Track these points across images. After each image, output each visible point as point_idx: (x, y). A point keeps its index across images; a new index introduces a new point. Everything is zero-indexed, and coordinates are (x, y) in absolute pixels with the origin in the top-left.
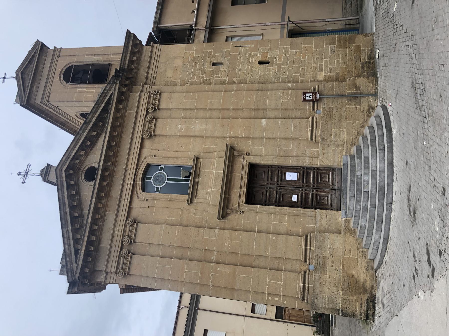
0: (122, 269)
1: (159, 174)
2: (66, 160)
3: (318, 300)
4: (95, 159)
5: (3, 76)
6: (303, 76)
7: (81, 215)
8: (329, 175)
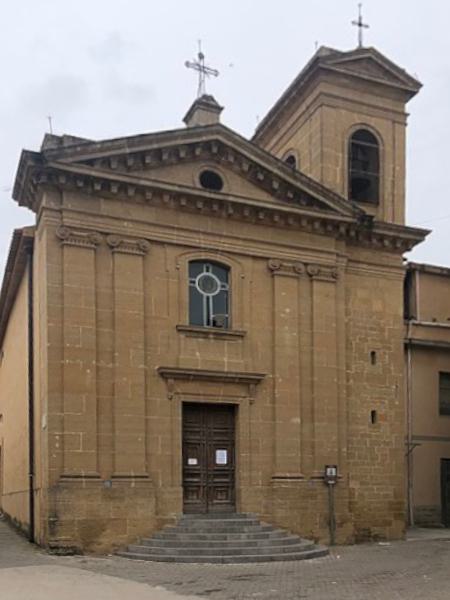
0: (71, 235)
2: (235, 141)
4: (236, 188)
5: (363, 22)
6: (355, 464)
7: (146, 167)
8: (226, 499)
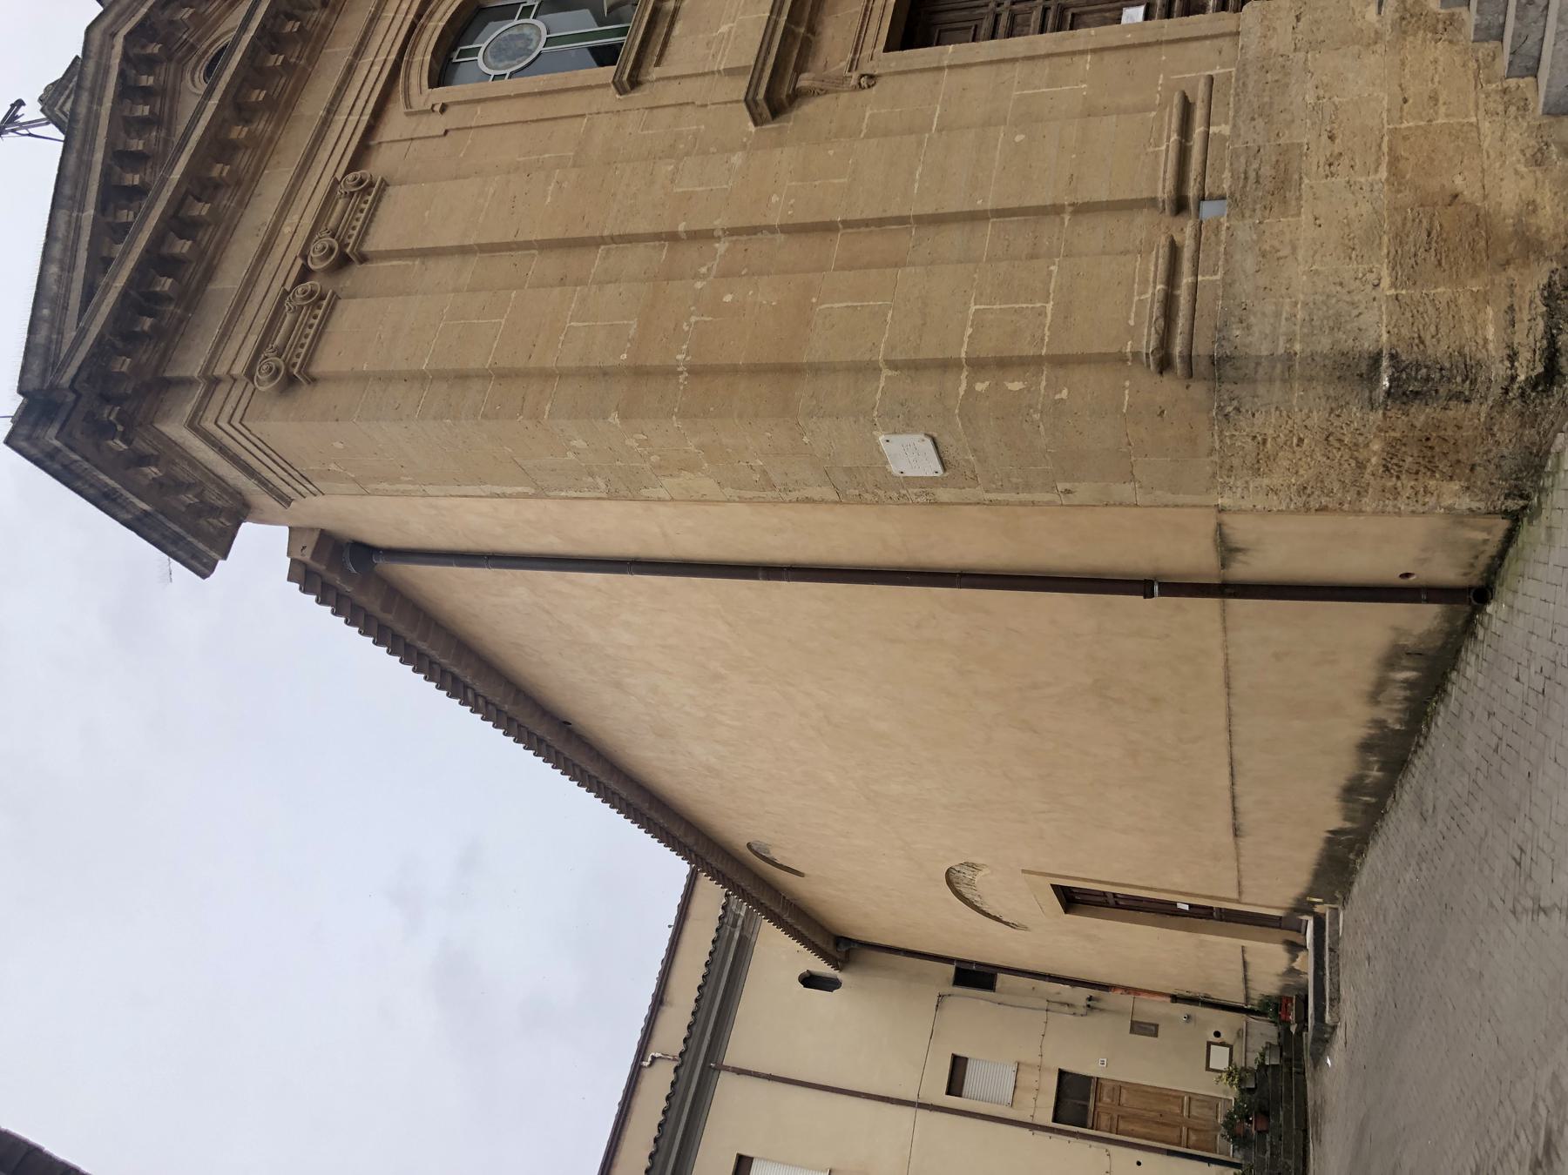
1: (515, 32)
3: (1249, 327)
